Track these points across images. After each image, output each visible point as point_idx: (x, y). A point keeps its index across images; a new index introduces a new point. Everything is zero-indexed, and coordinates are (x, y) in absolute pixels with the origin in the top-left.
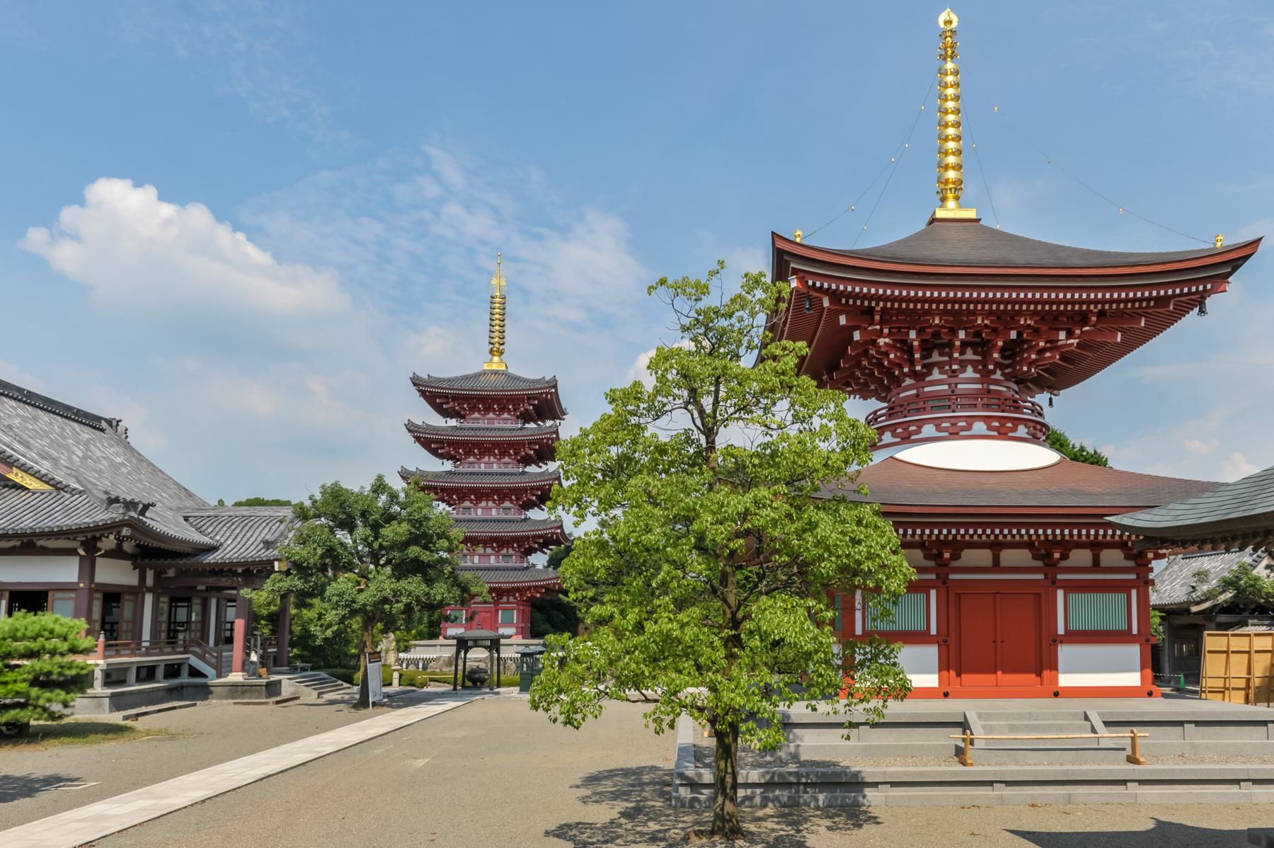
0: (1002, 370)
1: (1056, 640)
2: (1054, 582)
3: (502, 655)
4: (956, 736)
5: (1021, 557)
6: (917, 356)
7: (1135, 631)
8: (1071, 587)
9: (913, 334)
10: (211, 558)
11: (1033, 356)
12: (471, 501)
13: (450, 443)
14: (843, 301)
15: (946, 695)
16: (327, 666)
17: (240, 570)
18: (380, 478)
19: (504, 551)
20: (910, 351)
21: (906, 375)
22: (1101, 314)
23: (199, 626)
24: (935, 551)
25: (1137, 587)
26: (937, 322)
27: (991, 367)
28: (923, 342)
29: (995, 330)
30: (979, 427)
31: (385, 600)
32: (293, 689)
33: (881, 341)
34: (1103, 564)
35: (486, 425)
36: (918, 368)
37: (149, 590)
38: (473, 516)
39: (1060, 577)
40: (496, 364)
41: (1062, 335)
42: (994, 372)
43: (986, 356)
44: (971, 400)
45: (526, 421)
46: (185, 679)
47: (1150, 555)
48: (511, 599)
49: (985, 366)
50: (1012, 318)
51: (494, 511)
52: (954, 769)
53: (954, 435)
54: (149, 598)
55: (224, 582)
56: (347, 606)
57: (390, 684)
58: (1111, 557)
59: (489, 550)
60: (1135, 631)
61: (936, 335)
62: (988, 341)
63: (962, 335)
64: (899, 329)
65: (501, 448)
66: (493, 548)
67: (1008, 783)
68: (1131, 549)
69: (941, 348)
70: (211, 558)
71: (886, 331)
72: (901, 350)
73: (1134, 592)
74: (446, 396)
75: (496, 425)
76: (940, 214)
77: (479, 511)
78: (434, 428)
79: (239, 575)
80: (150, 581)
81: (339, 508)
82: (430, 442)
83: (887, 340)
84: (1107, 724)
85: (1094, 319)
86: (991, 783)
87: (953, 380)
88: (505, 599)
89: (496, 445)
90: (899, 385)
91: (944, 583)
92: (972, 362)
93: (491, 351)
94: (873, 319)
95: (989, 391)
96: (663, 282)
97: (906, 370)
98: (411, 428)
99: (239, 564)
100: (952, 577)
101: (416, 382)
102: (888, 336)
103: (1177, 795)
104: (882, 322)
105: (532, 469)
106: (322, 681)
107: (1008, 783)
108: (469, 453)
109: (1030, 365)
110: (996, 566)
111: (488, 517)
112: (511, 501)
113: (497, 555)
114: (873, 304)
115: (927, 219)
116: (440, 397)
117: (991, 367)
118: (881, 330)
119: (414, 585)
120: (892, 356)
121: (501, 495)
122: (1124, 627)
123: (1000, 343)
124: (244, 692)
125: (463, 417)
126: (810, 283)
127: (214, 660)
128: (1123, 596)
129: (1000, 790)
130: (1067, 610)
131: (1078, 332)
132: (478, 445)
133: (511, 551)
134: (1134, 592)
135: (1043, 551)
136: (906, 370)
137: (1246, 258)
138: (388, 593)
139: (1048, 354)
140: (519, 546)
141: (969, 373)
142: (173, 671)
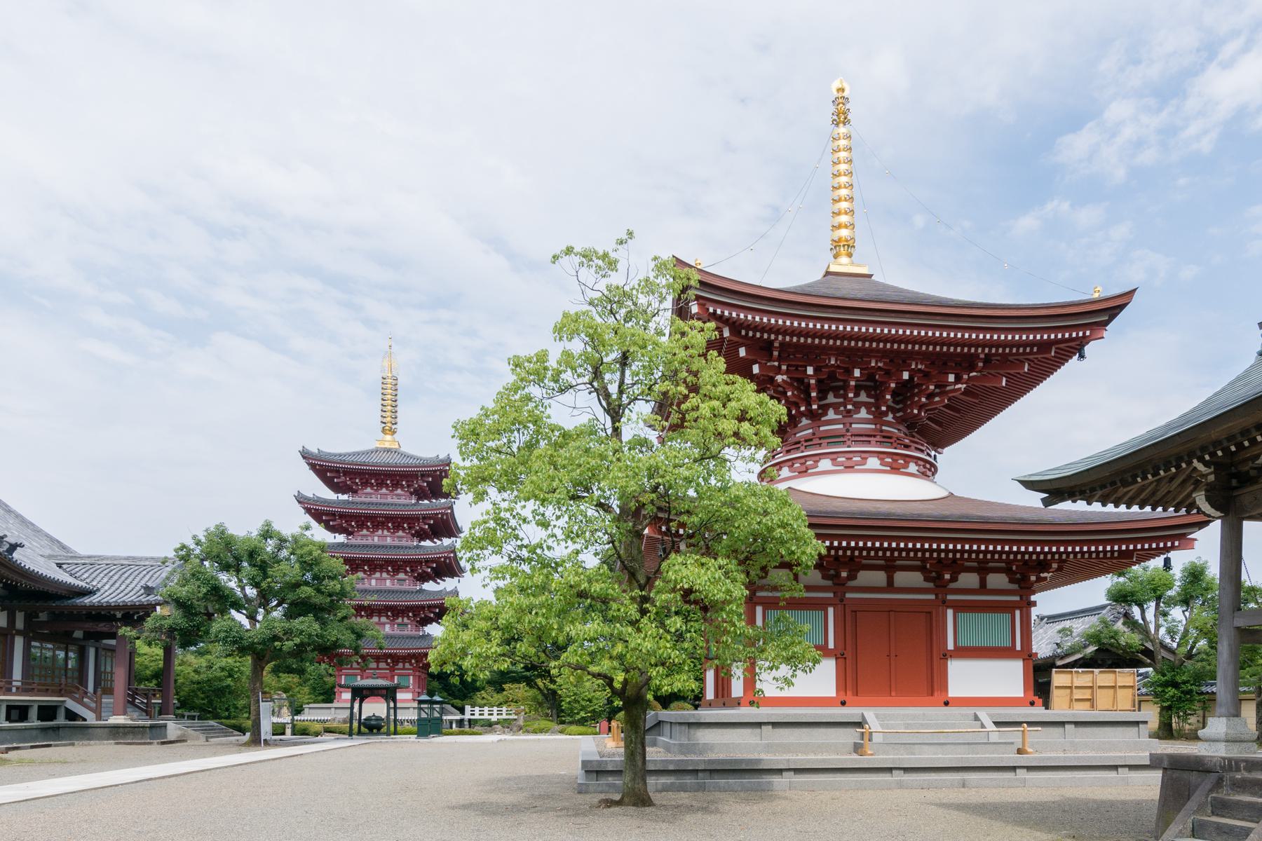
0: (894, 413)
1: (946, 655)
2: (944, 602)
3: (399, 717)
4: (851, 736)
5: (915, 579)
6: (814, 394)
7: (1018, 647)
8: (960, 607)
9: (810, 371)
10: (87, 601)
11: (923, 400)
12: (365, 571)
13: (342, 516)
14: (743, 332)
15: (843, 704)
16: (216, 717)
17: (119, 615)
18: (268, 524)
19: (400, 620)
20: (806, 389)
21: (802, 414)
22: (988, 360)
23: (76, 674)
24: (832, 572)
25: (1020, 608)
26: (833, 362)
27: (884, 408)
28: (819, 381)
29: (887, 373)
30: (873, 462)
31: (275, 638)
32: (179, 733)
33: (779, 378)
34: (989, 586)
35: (379, 500)
36: (815, 407)
37: (19, 633)
38: (367, 586)
39: (950, 597)
40: (388, 442)
41: (951, 378)
42: (886, 414)
43: (879, 399)
44: (865, 437)
45: (422, 539)
46: (61, 720)
47: (1033, 578)
48: (407, 665)
49: (878, 408)
50: (904, 362)
51: (388, 582)
52: (853, 760)
53: (849, 468)
54: (19, 642)
55: (102, 627)
56: (235, 642)
57: (283, 734)
58: (997, 580)
59: (383, 619)
60: (1018, 647)
61: (832, 377)
62: (882, 383)
63: (857, 373)
64: (797, 366)
65: (396, 522)
66: (388, 617)
67: (906, 770)
68: (1015, 573)
69: (836, 391)
70: (87, 601)
71: (784, 367)
72: (798, 389)
73: (1018, 613)
74: (337, 471)
75: (389, 500)
76: (833, 269)
77: (373, 582)
78: (325, 501)
79: (119, 620)
80: (20, 624)
81: (226, 552)
82: (320, 513)
83: (785, 377)
84: (997, 724)
85: (981, 364)
86: (890, 770)
87: (847, 420)
88: (400, 665)
89: (390, 518)
90: (796, 426)
91: (842, 600)
92: (866, 405)
93: (384, 430)
94: (772, 354)
95: (882, 431)
96: (569, 251)
97: (803, 409)
98: (301, 500)
99: (117, 607)
100: (848, 595)
101: (306, 455)
102: (787, 372)
103: (1061, 779)
104: (780, 359)
105: (427, 543)
106: (212, 728)
107: (906, 770)
108: (362, 525)
109: (921, 408)
110: (890, 586)
111: (382, 587)
112: (406, 572)
113: (392, 623)
114: (773, 337)
115: (823, 273)
116: (331, 471)
117: (884, 408)
118: (779, 367)
119: (307, 624)
120: (789, 394)
121: (395, 566)
122: (1008, 644)
123: (893, 385)
124: (125, 734)
125: (355, 492)
126: (711, 310)
127: (93, 705)
128: (1008, 616)
129: (898, 776)
130: (952, 628)
131: (965, 377)
132: (372, 518)
133: (406, 620)
134: (1018, 613)
135: (934, 574)
136: (803, 409)
137: (1121, 307)
138: (278, 631)
139: (937, 399)
140: (414, 616)
141: (863, 413)
142: (47, 712)
